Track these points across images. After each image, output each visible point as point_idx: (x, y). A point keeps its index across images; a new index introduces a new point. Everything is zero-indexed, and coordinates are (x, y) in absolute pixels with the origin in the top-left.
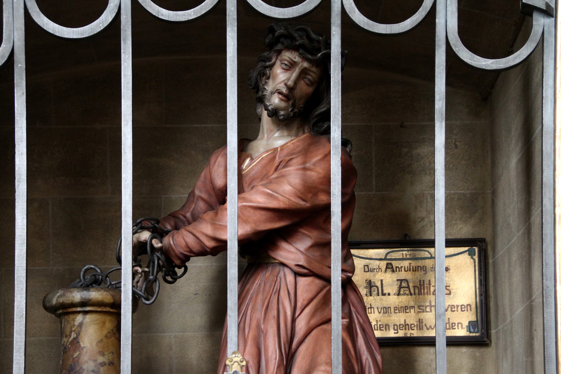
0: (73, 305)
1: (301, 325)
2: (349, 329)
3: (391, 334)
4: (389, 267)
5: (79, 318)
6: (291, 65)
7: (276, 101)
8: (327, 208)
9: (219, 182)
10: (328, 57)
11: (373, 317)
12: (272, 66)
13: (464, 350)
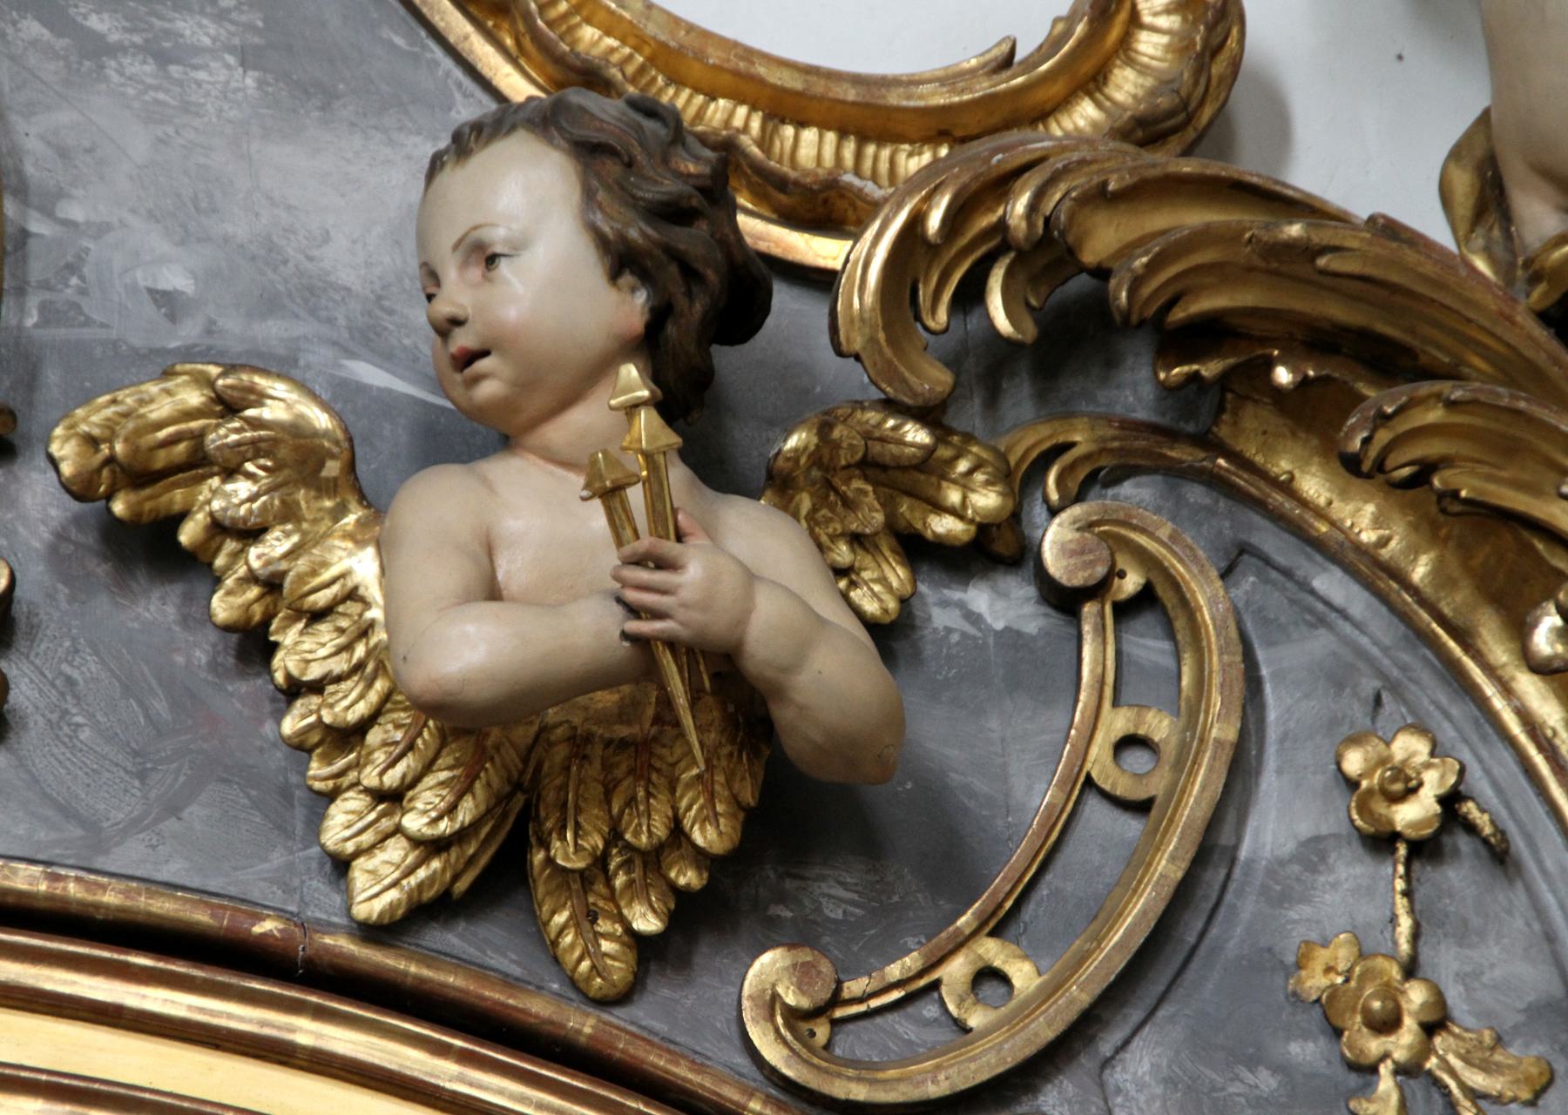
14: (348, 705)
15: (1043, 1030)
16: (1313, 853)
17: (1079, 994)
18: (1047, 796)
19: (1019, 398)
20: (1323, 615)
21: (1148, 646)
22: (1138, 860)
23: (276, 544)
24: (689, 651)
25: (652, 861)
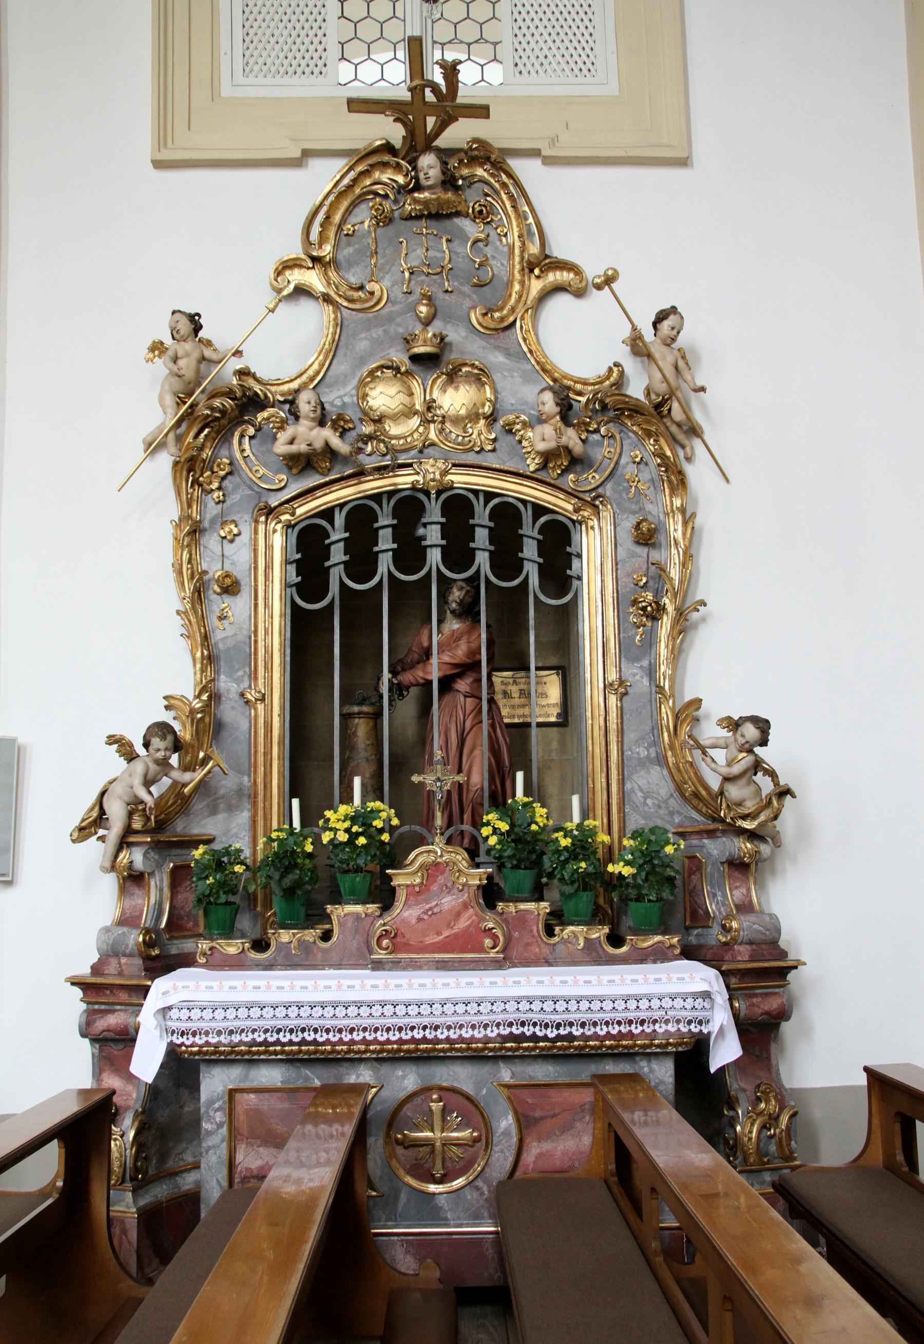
0: (354, 714)
1: (468, 724)
2: (493, 726)
3: (516, 720)
4: (515, 682)
5: (357, 720)
6: (461, 589)
7: (454, 605)
8: (480, 662)
9: (426, 644)
10: (479, 585)
11: (504, 712)
12: (452, 588)
13: (555, 729)
14: (529, 449)
15: (599, 483)
16: (627, 463)
17: (602, 479)
18: (600, 458)
19: (599, 414)
20: (629, 438)
21: (612, 441)
22: (609, 465)
23: (522, 432)
24: (563, 447)
25: (560, 466)
